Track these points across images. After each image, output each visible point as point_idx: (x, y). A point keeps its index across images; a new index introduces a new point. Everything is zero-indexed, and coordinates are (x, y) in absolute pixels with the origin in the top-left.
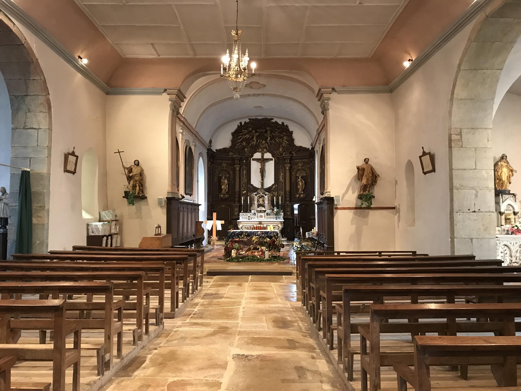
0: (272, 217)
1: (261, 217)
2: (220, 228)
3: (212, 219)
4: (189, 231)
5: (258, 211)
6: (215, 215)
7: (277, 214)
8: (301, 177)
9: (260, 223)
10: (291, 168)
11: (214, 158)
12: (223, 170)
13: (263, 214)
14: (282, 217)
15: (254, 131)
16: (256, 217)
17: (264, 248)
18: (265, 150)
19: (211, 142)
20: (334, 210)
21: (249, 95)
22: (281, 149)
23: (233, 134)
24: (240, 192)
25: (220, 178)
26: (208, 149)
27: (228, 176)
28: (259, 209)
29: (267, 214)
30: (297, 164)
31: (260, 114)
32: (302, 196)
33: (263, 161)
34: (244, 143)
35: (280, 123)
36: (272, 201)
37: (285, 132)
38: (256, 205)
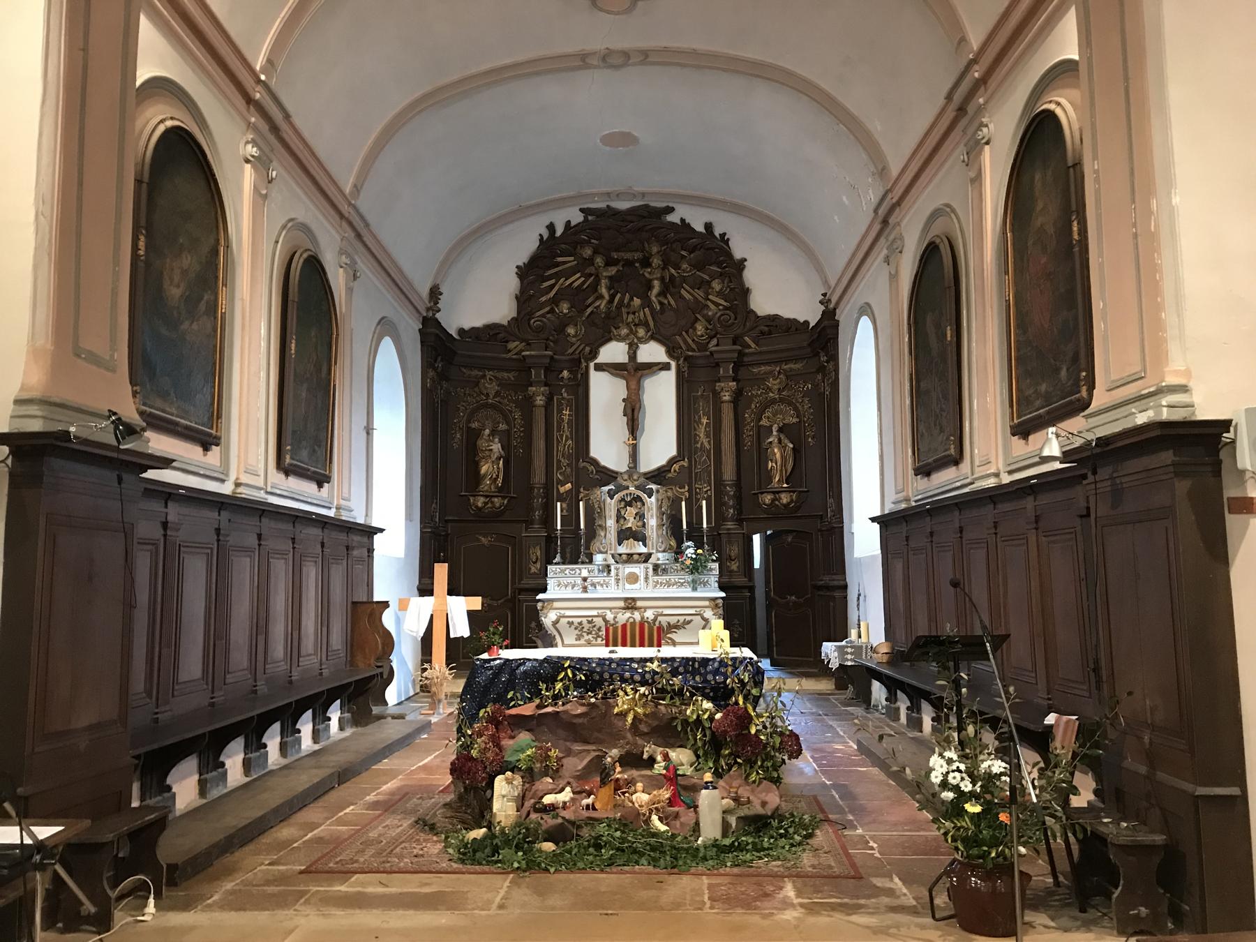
0: (673, 578)
1: (633, 579)
2: (461, 629)
3: (431, 594)
4: (309, 644)
5: (618, 558)
6: (441, 572)
7: (697, 567)
8: (780, 430)
9: (630, 604)
10: (738, 395)
11: (450, 368)
12: (487, 406)
13: (638, 569)
14: (713, 580)
15: (599, 260)
16: (612, 581)
17: (682, 757)
18: (641, 332)
19: (435, 293)
20: (1232, 520)
21: (583, 61)
22: (700, 329)
23: (523, 272)
24: (549, 486)
25: (473, 437)
26: (425, 321)
27: (503, 427)
28: (622, 550)
29: (656, 568)
30: (760, 380)
31: (626, 183)
32: (785, 498)
33: (633, 373)
34: (565, 307)
35: (700, 228)
36: (674, 521)
37: (715, 258)
38: (612, 535)
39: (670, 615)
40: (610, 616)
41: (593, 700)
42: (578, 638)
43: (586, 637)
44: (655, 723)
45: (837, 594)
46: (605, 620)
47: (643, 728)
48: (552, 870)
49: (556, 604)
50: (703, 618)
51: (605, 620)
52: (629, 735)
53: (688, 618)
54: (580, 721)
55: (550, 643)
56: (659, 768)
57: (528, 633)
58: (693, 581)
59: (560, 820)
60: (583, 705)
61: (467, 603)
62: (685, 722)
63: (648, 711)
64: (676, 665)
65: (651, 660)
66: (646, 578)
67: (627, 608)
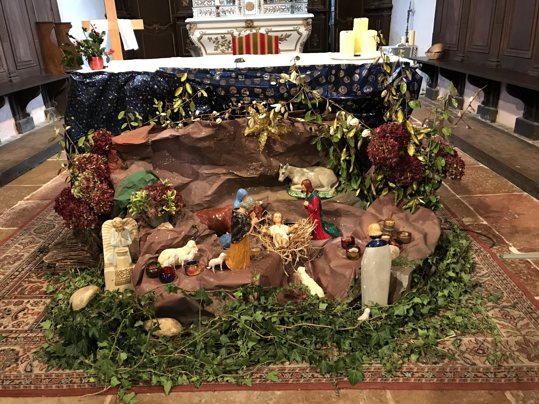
9: (249, 24)
16: (237, 9)
17: (322, 177)
39: (277, 30)
40: (236, 33)
41: (219, 121)
42: (216, 49)
43: (221, 48)
44: (291, 143)
45: (385, 13)
46: (232, 35)
47: (278, 148)
48: (168, 386)
49: (199, 26)
50: (299, 33)
51: (232, 35)
52: (262, 158)
53: (289, 33)
54: (206, 144)
55: (198, 54)
56: (296, 191)
57: (185, 46)
58: (292, 7)
59: (179, 295)
60: (207, 126)
61: (133, 24)
62: (327, 142)
63: (285, 131)
64: (317, 74)
65: (286, 70)
66: (260, 6)
67: (247, 27)
